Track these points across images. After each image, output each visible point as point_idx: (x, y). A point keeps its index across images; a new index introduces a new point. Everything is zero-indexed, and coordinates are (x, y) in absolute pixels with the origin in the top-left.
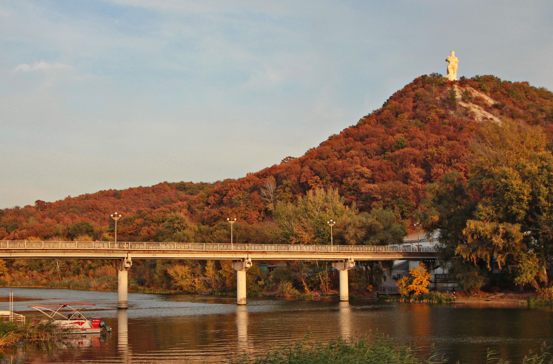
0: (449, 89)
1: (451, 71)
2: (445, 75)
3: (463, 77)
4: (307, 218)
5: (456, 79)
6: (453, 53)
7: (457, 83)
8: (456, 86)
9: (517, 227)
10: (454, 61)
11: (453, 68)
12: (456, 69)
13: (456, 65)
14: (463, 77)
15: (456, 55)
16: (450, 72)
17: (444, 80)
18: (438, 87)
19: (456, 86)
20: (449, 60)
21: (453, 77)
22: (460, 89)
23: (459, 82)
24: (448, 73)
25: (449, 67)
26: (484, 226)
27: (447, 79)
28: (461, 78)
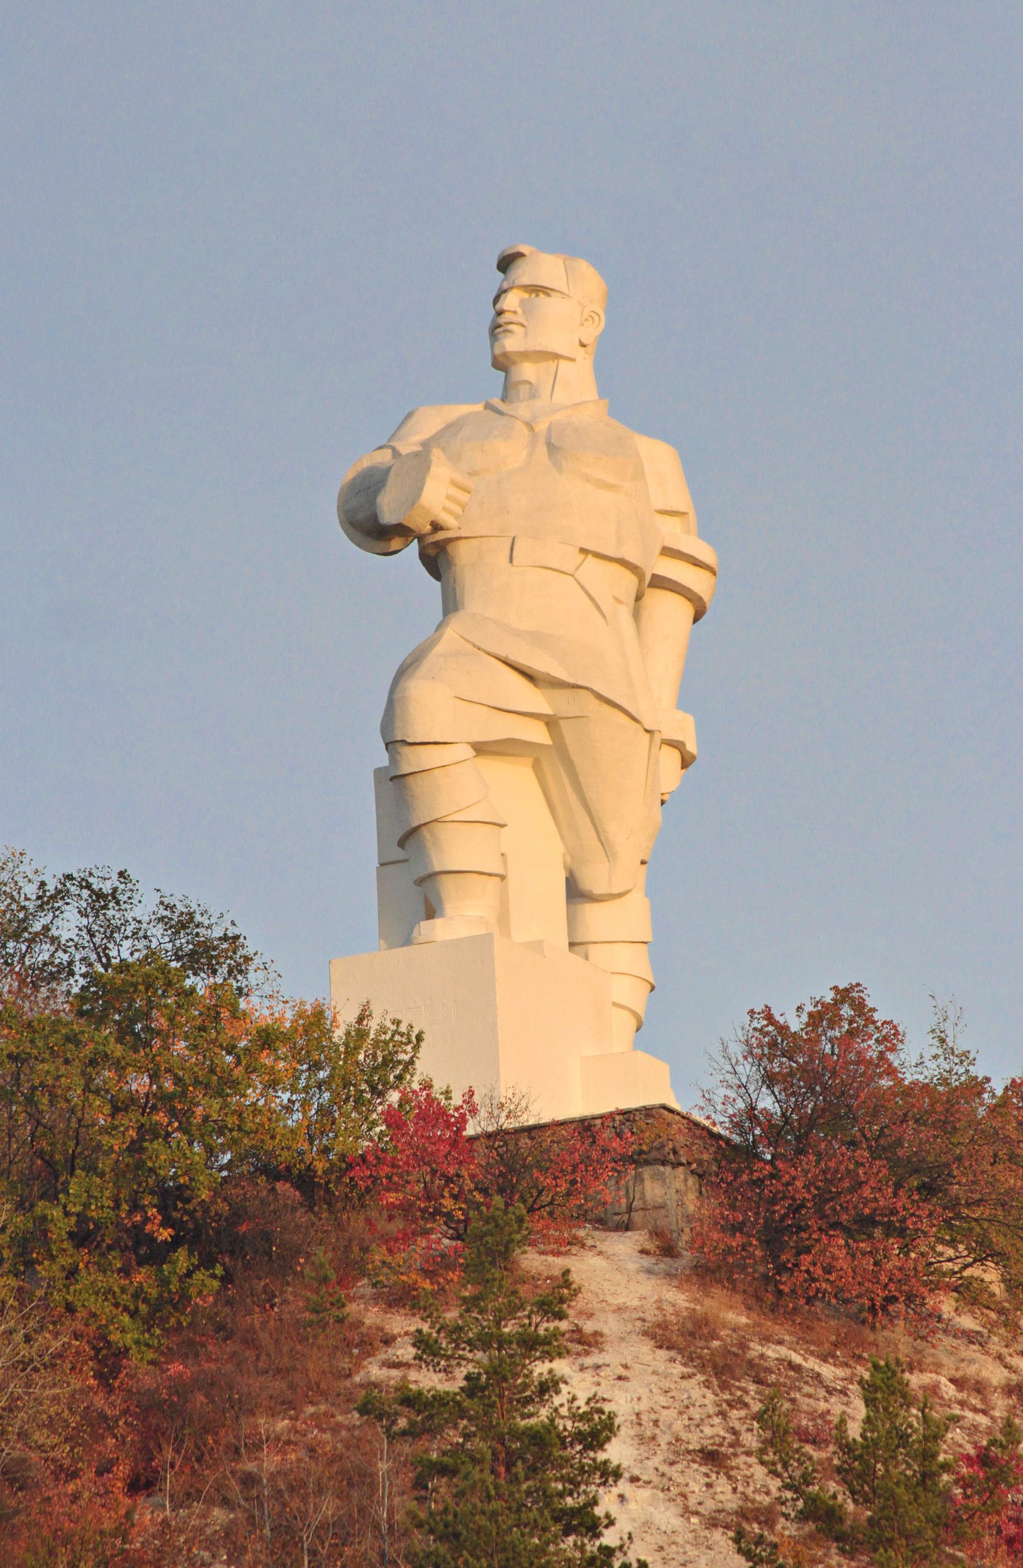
0: (402, 1357)
1: (496, 824)
2: (314, 962)
3: (845, 1009)
4: (157, 1255)
5: (644, 1083)
6: (565, 310)
7: (670, 1192)
8: (613, 1277)
9: (778, 1483)
10: (579, 523)
11: (556, 757)
12: (636, 784)
13: (651, 663)
14: (845, 1009)
15: (631, 387)
16: (454, 850)
17: (285, 1105)
18: (100, 1289)
19: (613, 1277)
20: (437, 498)
21: (559, 1012)
22: (724, 1368)
23: (723, 1159)
24: (411, 878)
25: (437, 708)
26: (685, 1553)
27: (387, 1057)
28: (775, 1046)
